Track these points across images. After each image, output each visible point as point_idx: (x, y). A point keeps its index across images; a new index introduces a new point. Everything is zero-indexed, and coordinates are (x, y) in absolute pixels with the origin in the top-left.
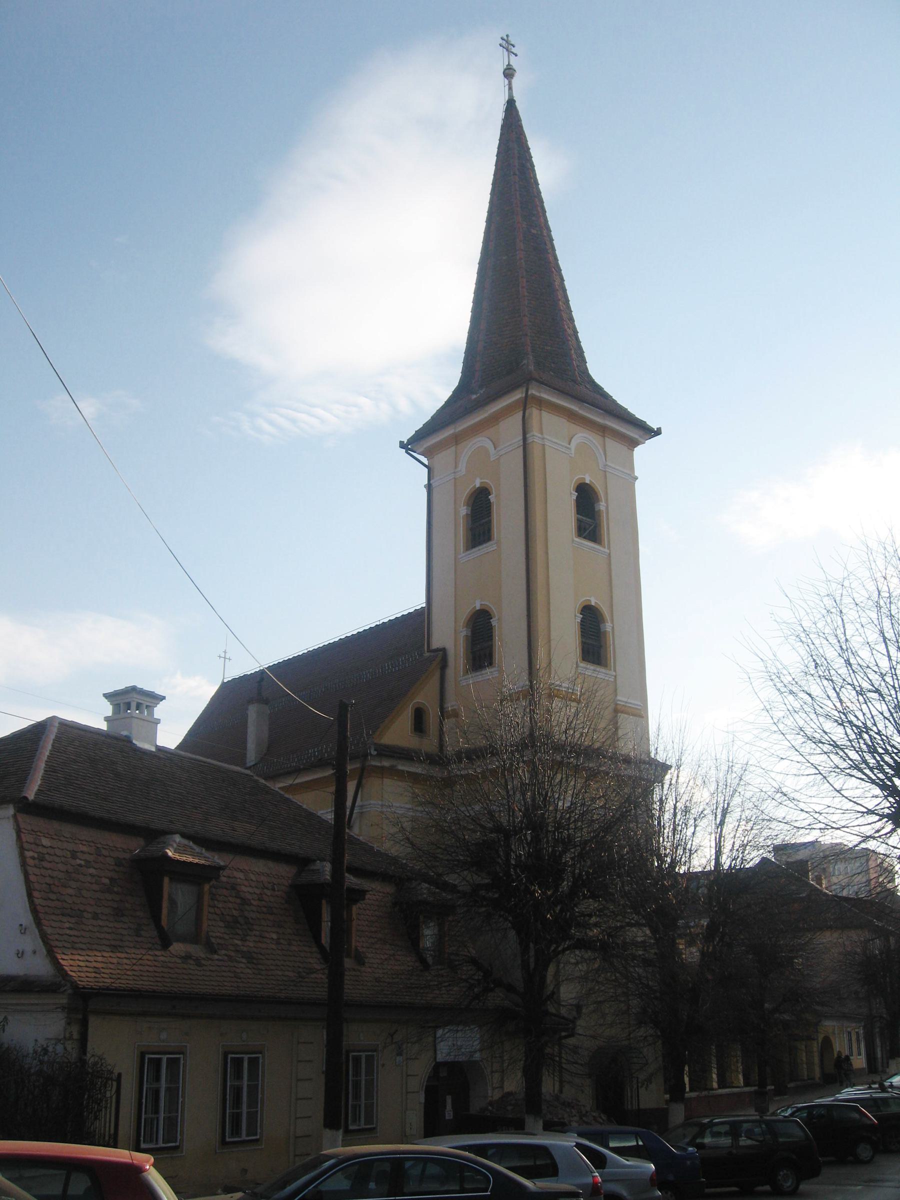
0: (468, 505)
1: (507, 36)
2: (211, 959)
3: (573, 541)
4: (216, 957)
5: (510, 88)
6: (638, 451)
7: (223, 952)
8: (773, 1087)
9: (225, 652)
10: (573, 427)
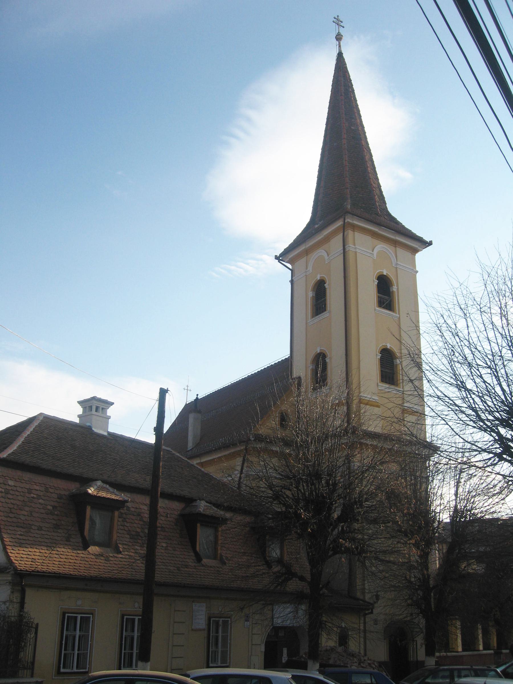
0: (313, 291)
1: (338, 16)
2: (116, 557)
3: (375, 309)
4: (121, 556)
5: (340, 46)
6: (418, 256)
9: (187, 386)
10: (376, 241)
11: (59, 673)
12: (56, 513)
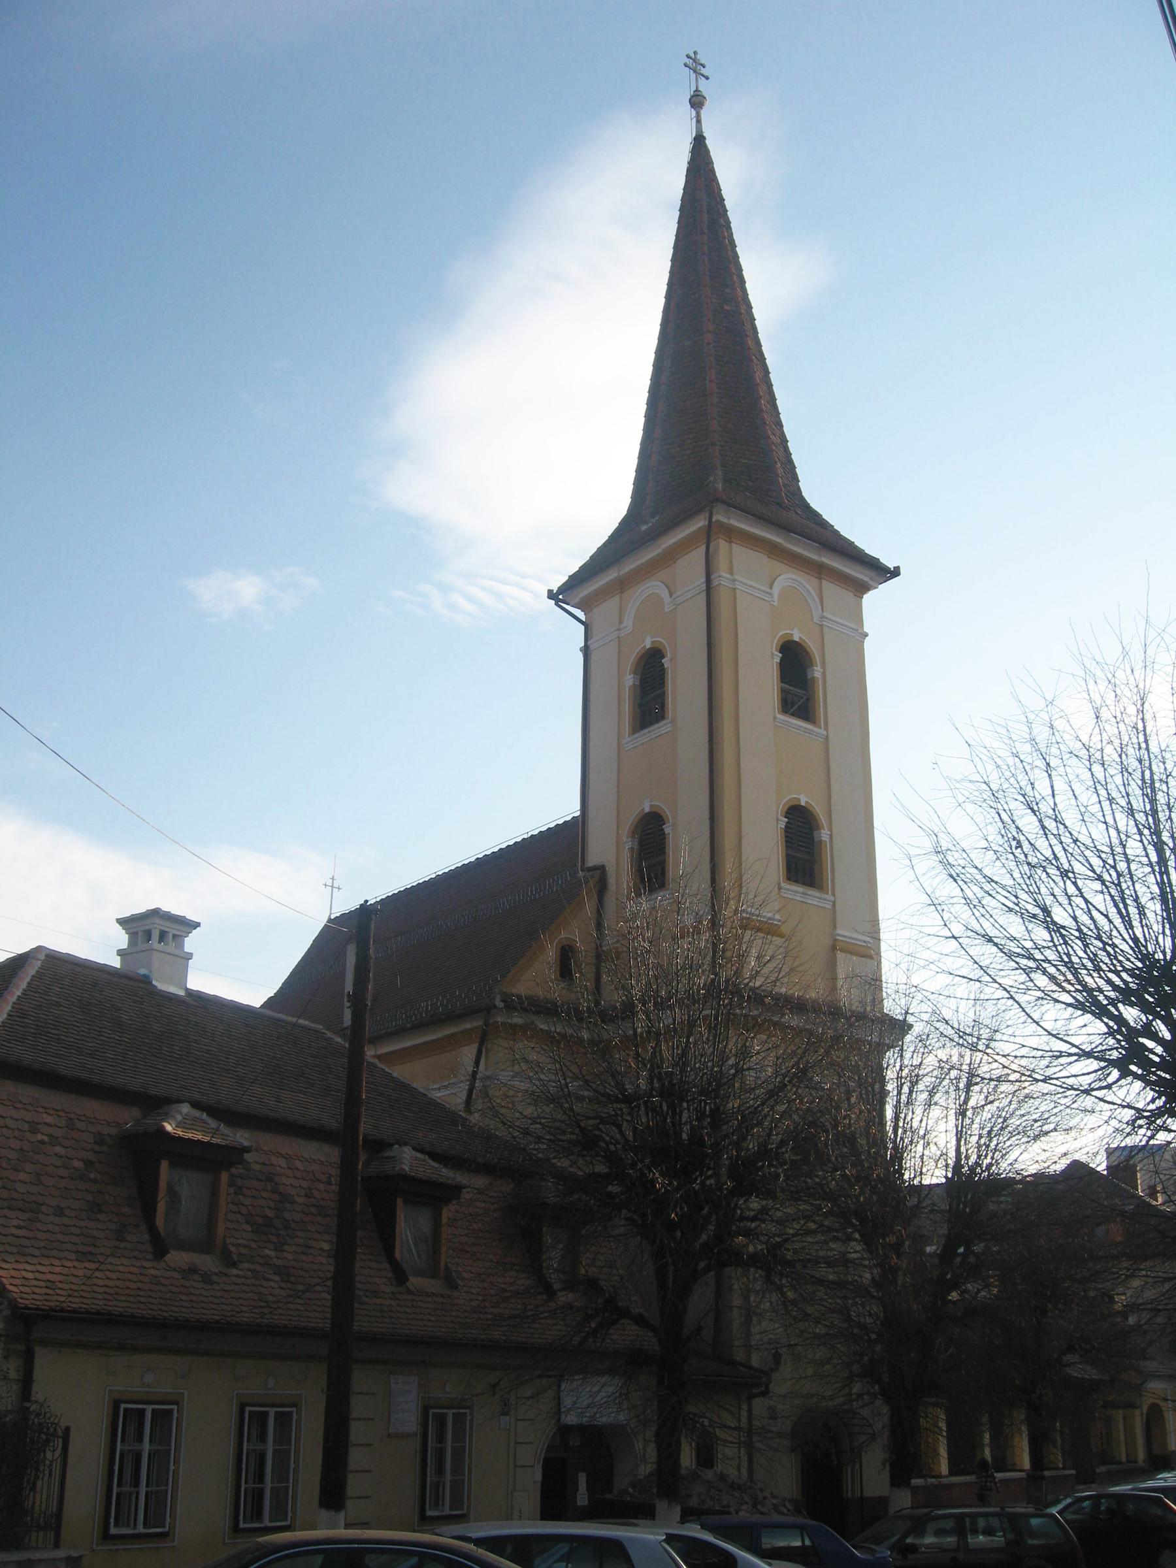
0: (635, 673)
1: (695, 53)
3: (775, 718)
4: (235, 1272)
5: (699, 121)
6: (869, 599)
7: (246, 1265)
8: (1073, 1472)
9: (333, 879)
10: (778, 566)
11: (106, 1536)
12: (92, 1176)
